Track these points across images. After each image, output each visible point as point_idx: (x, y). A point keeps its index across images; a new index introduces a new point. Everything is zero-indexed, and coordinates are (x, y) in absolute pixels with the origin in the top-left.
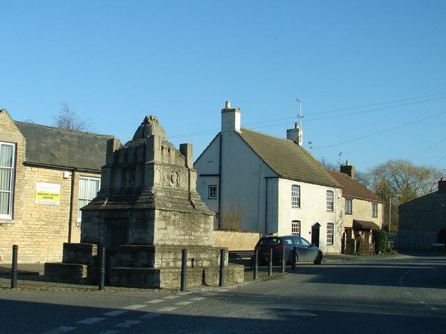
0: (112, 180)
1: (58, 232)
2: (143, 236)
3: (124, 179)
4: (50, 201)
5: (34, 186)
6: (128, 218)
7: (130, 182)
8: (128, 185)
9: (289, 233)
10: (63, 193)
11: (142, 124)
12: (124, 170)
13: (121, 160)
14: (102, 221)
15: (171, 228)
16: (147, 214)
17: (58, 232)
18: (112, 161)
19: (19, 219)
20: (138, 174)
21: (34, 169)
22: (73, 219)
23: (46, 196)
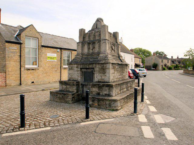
0: (82, 49)
1: (56, 71)
2: (103, 77)
3: (89, 49)
4: (53, 60)
5: (46, 54)
6: (94, 68)
7: (92, 50)
8: (91, 51)
9: (48, 56)
10: (58, 57)
11: (96, 22)
12: (89, 44)
13: (87, 39)
14: (79, 69)
15: (116, 72)
16: (105, 66)
17: (56, 71)
18: (82, 40)
19: (41, 67)
20: (97, 46)
21: (46, 48)
22: (62, 66)
23: (51, 58)
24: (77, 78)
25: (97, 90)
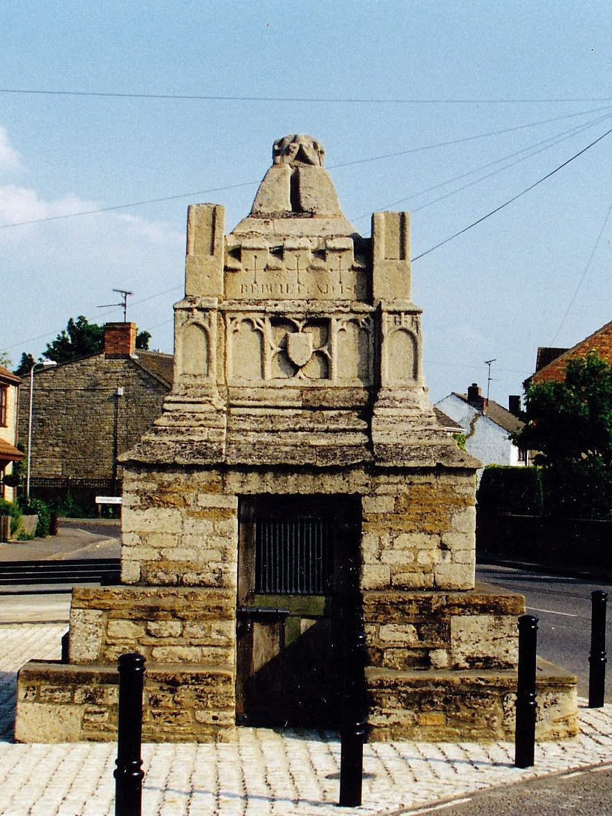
14: (234, 503)
24: (213, 566)
25: (412, 639)
